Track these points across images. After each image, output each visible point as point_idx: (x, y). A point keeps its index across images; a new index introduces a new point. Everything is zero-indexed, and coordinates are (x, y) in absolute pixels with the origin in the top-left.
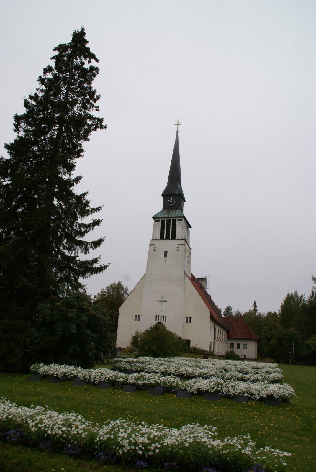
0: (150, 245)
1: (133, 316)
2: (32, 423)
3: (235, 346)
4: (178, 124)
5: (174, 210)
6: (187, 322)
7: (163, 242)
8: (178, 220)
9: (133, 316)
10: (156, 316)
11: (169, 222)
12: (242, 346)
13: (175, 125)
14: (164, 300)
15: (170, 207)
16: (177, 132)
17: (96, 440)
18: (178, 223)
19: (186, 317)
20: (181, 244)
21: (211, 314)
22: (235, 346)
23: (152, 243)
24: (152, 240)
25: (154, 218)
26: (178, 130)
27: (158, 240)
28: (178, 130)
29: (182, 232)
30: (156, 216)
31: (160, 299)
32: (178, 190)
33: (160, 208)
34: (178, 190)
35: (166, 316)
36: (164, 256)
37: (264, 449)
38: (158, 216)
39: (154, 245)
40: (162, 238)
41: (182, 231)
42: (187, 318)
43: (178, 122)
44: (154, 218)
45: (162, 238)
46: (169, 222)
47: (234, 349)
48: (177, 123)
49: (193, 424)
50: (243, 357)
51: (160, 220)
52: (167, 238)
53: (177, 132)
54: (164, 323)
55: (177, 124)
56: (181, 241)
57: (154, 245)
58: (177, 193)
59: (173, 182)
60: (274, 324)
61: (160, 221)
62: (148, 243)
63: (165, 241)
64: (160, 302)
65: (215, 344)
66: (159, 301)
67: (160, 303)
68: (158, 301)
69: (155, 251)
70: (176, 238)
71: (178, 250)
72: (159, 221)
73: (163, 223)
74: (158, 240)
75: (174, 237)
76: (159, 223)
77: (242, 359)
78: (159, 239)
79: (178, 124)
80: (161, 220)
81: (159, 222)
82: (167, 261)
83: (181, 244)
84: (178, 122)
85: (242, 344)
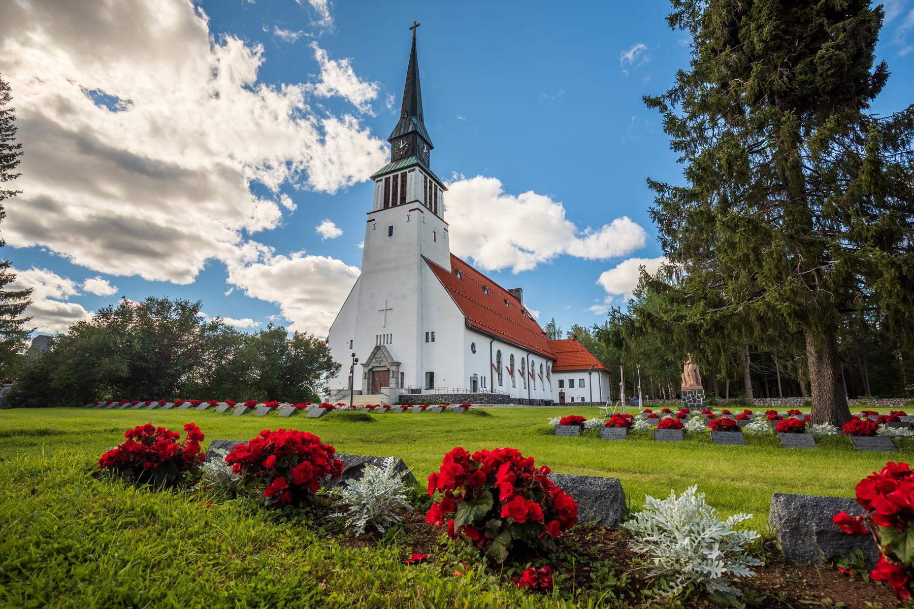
2: (20, 174)
3: (566, 384)
11: (396, 178)
14: (389, 307)
16: (414, 39)
17: (225, 359)
18: (409, 175)
22: (566, 384)
23: (372, 217)
37: (182, 346)
39: (374, 220)
40: (386, 206)
42: (427, 334)
43: (415, 22)
45: (386, 206)
46: (396, 178)
48: (412, 25)
49: (885, 471)
50: (580, 401)
51: (383, 178)
52: (395, 205)
53: (414, 39)
54: (388, 346)
57: (374, 220)
60: (66, 583)
61: (384, 180)
72: (381, 180)
73: (387, 180)
75: (404, 201)
76: (382, 184)
84: (415, 22)
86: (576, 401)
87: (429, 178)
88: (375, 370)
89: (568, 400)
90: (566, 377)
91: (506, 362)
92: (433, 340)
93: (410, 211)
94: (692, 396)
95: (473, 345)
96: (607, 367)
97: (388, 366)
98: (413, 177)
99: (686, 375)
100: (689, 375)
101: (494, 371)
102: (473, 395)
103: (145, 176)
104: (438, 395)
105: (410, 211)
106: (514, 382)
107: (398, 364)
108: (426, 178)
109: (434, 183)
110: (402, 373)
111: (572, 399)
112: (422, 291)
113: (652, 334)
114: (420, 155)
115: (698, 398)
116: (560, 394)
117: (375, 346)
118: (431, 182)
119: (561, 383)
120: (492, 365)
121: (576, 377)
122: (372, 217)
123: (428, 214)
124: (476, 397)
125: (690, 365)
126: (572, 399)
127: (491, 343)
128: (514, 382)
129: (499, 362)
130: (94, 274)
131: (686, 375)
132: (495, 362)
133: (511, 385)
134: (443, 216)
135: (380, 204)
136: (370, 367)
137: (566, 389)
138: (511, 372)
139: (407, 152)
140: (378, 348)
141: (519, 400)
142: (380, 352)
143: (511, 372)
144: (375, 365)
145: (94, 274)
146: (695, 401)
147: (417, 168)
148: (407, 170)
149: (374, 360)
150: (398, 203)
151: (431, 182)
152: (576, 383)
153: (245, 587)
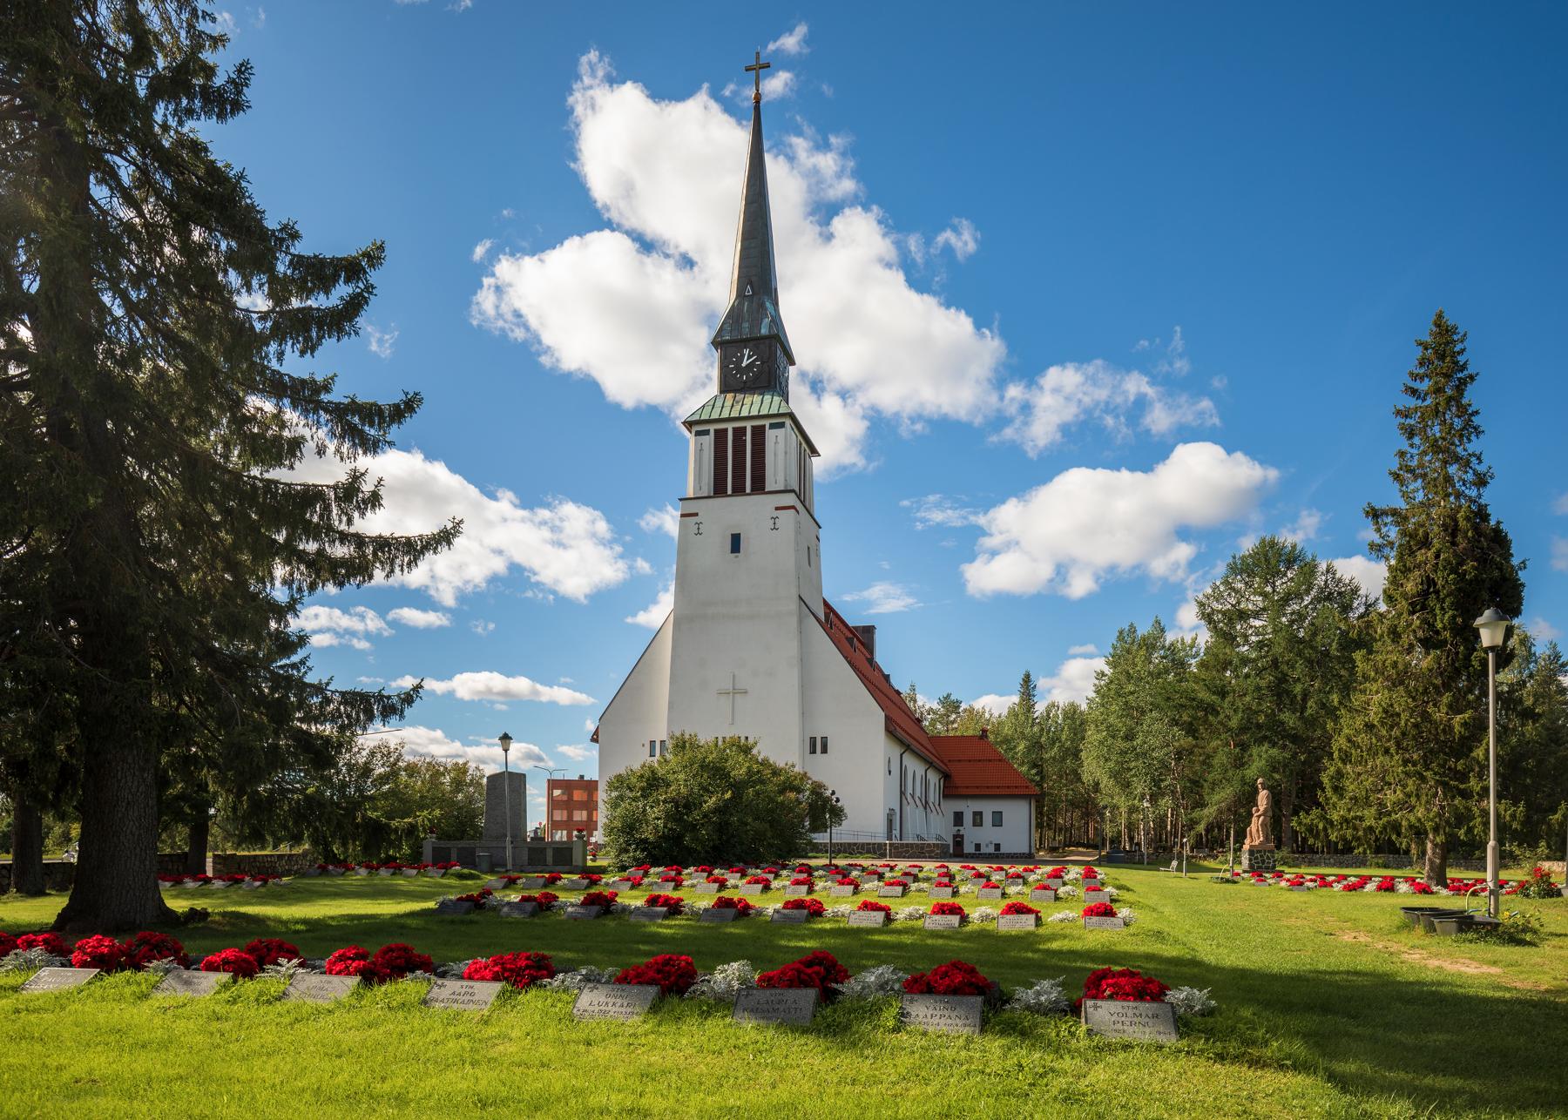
8: (773, 426)
11: (740, 433)
18: (771, 435)
22: (968, 819)
23: (692, 507)
30: (696, 417)
39: (696, 515)
40: (719, 490)
45: (719, 490)
46: (740, 433)
50: (991, 850)
51: (712, 428)
52: (739, 490)
55: (738, 139)
57: (696, 515)
61: (712, 432)
72: (707, 432)
73: (720, 436)
75: (759, 486)
76: (709, 441)
77: (990, 854)
86: (984, 850)
89: (969, 848)
90: (968, 808)
92: (824, 750)
93: (777, 509)
94: (1261, 856)
96: (1206, 835)
98: (781, 440)
99: (1254, 830)
100: (1258, 830)
102: (917, 845)
103: (795, 644)
104: (855, 844)
105: (777, 509)
111: (978, 846)
112: (804, 662)
115: (1268, 857)
116: (955, 837)
119: (958, 818)
121: (987, 808)
122: (692, 507)
124: (922, 848)
125: (1262, 818)
126: (978, 846)
127: (901, 755)
130: (1350, 876)
131: (1254, 830)
135: (707, 486)
137: (968, 830)
139: (757, 377)
145: (1350, 876)
146: (1263, 862)
148: (767, 423)
152: (988, 819)
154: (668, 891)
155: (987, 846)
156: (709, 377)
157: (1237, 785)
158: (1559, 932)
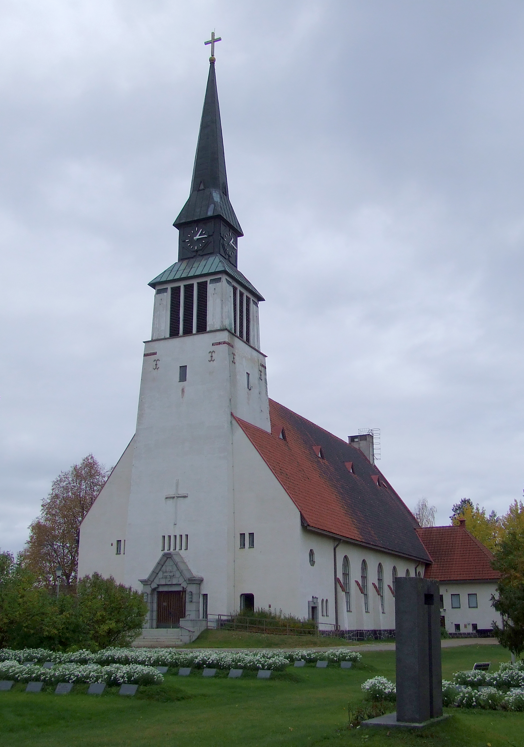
0: (145, 355)
1: (112, 545)
4: (213, 41)
5: (205, 257)
6: (243, 545)
7: (176, 342)
8: (212, 281)
9: (112, 545)
10: (164, 537)
11: (189, 289)
12: (464, 600)
13: (206, 43)
14: (182, 492)
15: (197, 251)
16: (212, 62)
18: (210, 288)
19: (241, 534)
20: (220, 343)
21: (303, 518)
24: (152, 341)
25: (153, 285)
26: (213, 56)
27: (165, 339)
28: (213, 56)
29: (222, 313)
30: (158, 280)
31: (172, 493)
32: (212, 206)
33: (173, 257)
34: (212, 206)
35: (187, 536)
36: (178, 379)
38: (164, 279)
39: (155, 354)
40: (174, 333)
41: (222, 308)
42: (243, 535)
43: (213, 34)
44: (153, 285)
45: (174, 333)
46: (189, 289)
47: (445, 610)
50: (470, 630)
51: (169, 287)
52: (188, 331)
53: (212, 62)
56: (218, 334)
57: (155, 354)
58: (210, 213)
59: (202, 187)
61: (169, 291)
62: (141, 349)
63: (196, 337)
64: (171, 500)
65: (339, 601)
66: (171, 498)
67: (170, 501)
68: (167, 498)
69: (156, 368)
70: (208, 329)
71: (212, 360)
72: (165, 290)
73: (175, 292)
74: (165, 339)
75: (202, 328)
76: (167, 297)
77: (469, 634)
78: (168, 336)
79: (213, 41)
80: (172, 288)
81: (165, 294)
82: (185, 390)
83: (220, 343)
84: (213, 34)
85: (464, 592)
86: (463, 630)
87: (239, 288)
88: (161, 589)
91: (355, 574)
92: (252, 545)
95: (312, 553)
97: (184, 585)
101: (339, 589)
106: (366, 604)
107: (200, 582)
108: (235, 289)
109: (246, 294)
110: (205, 596)
111: (458, 626)
113: (515, 556)
114: (225, 251)
117: (161, 554)
118: (241, 294)
120: (337, 580)
123: (239, 344)
126: (458, 626)
127: (335, 549)
128: (366, 604)
129: (346, 575)
132: (340, 576)
133: (364, 610)
134: (259, 347)
136: (154, 586)
138: (363, 589)
139: (206, 246)
140: (167, 557)
141: (375, 632)
142: (169, 562)
143: (363, 589)
144: (163, 582)
147: (224, 278)
148: (208, 279)
149: (160, 575)
150: (194, 330)
151: (241, 294)
153: (514, 540)
154: (307, 656)
155: (465, 626)
156: (227, 285)
157: (493, 544)
158: (212, 262)
